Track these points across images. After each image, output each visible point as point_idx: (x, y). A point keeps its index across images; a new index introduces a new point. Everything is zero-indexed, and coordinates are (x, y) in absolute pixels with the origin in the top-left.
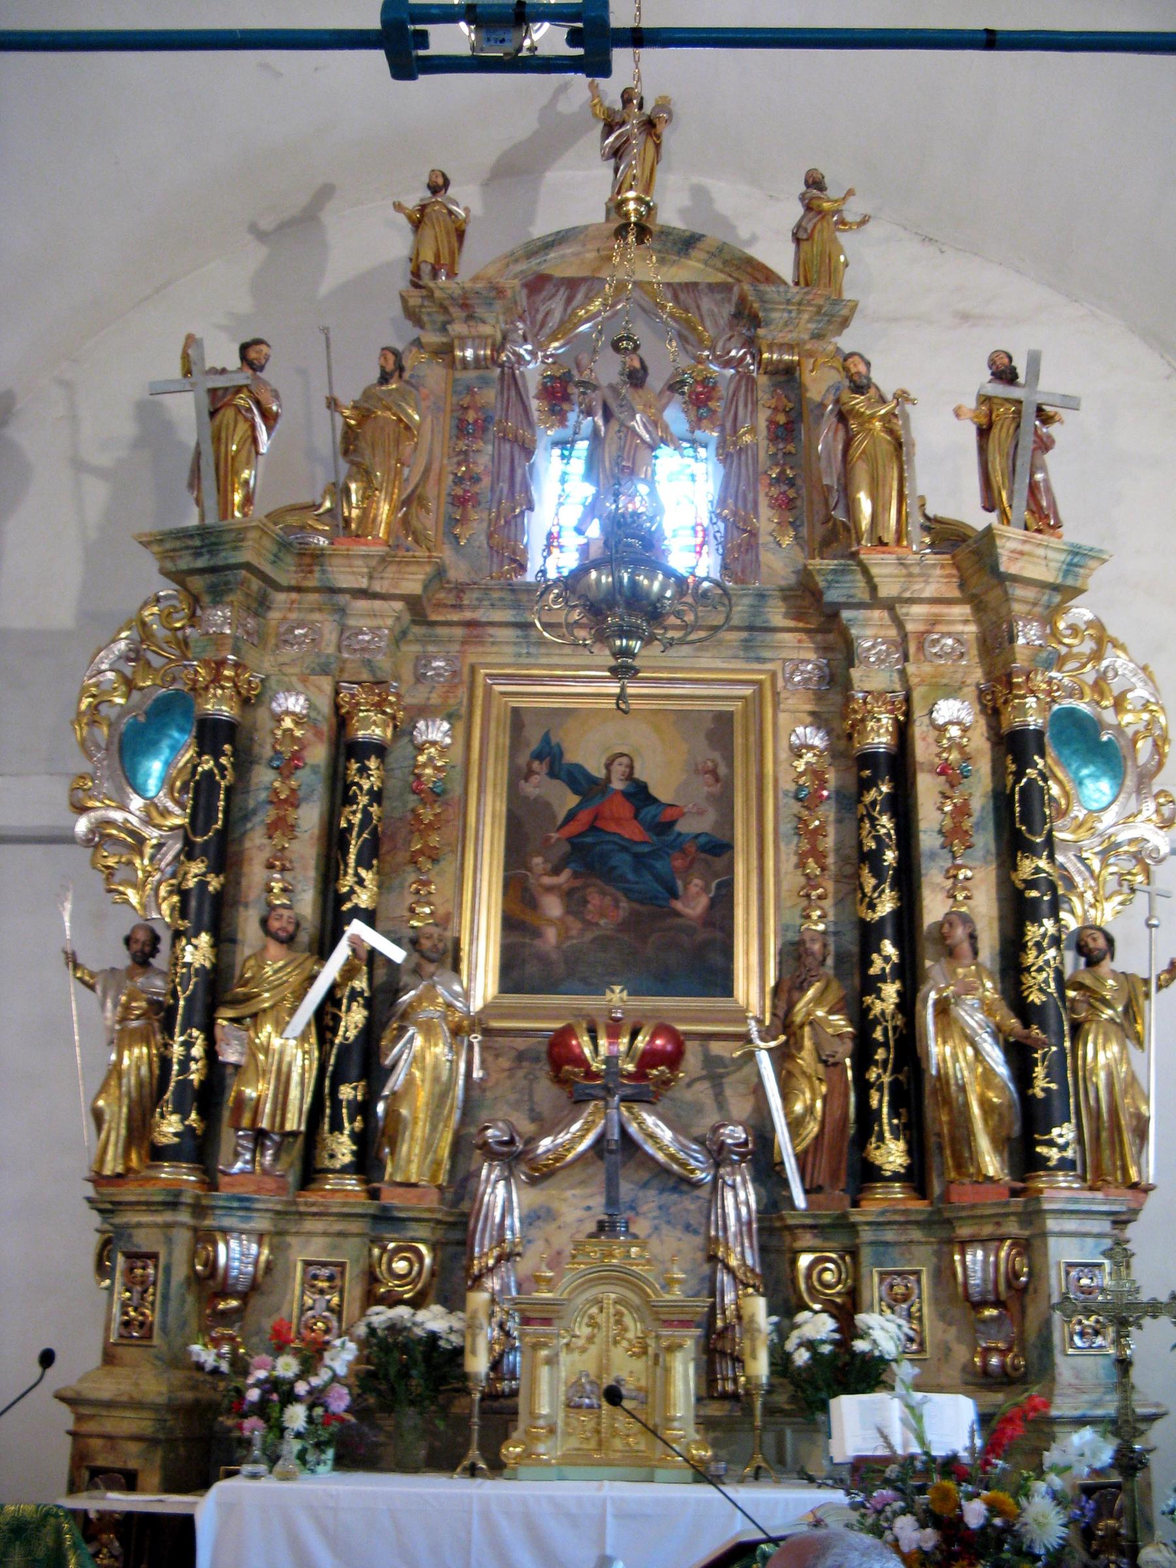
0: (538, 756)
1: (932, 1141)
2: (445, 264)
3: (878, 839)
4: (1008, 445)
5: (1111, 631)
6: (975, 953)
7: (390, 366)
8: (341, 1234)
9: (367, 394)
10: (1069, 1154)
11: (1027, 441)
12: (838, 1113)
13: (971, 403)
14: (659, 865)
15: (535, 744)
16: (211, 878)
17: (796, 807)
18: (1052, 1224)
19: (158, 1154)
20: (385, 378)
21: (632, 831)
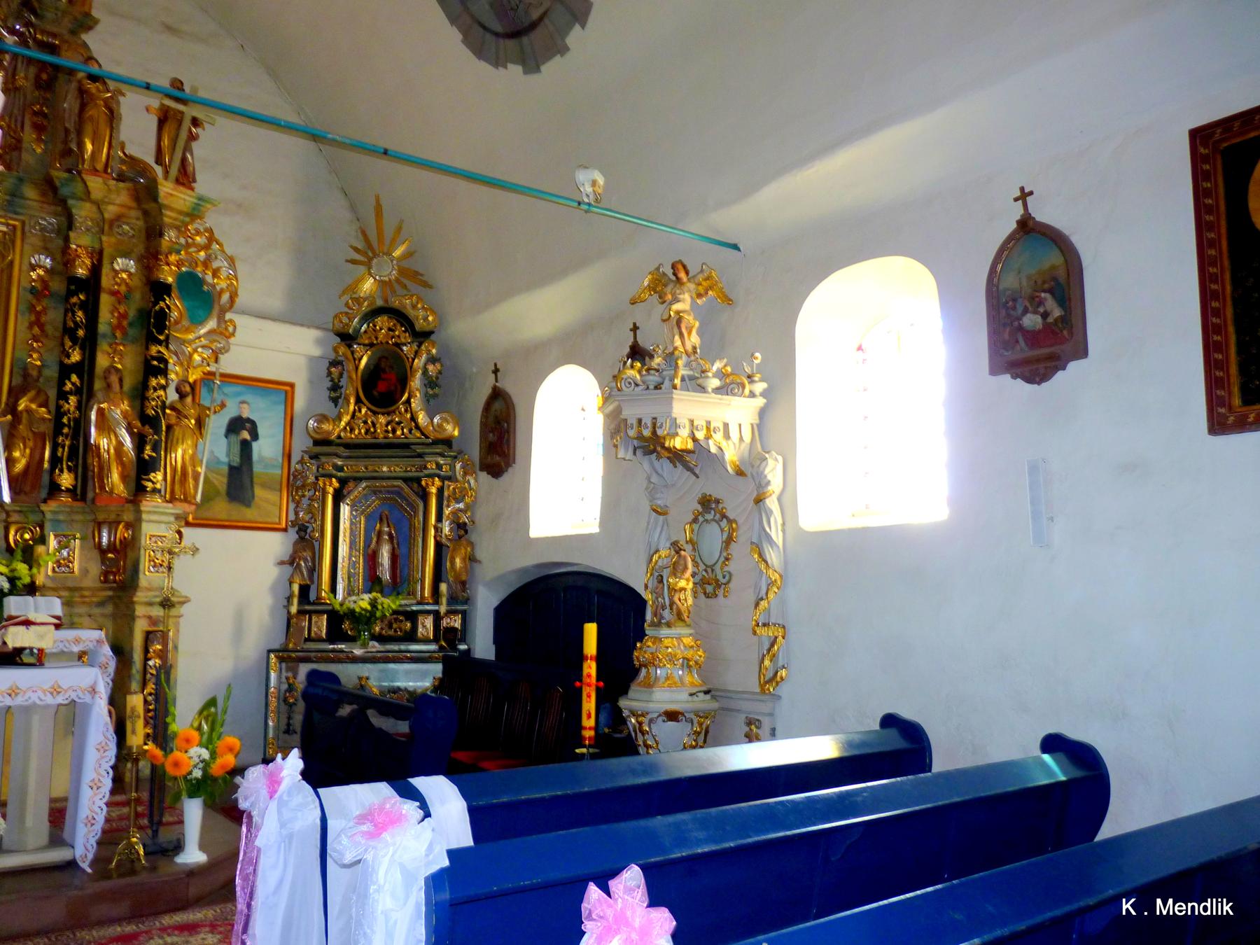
1: (90, 473)
5: (217, 235)
6: (121, 387)
10: (158, 486)
11: (183, 135)
12: (37, 457)
17: (30, 297)
18: (144, 516)
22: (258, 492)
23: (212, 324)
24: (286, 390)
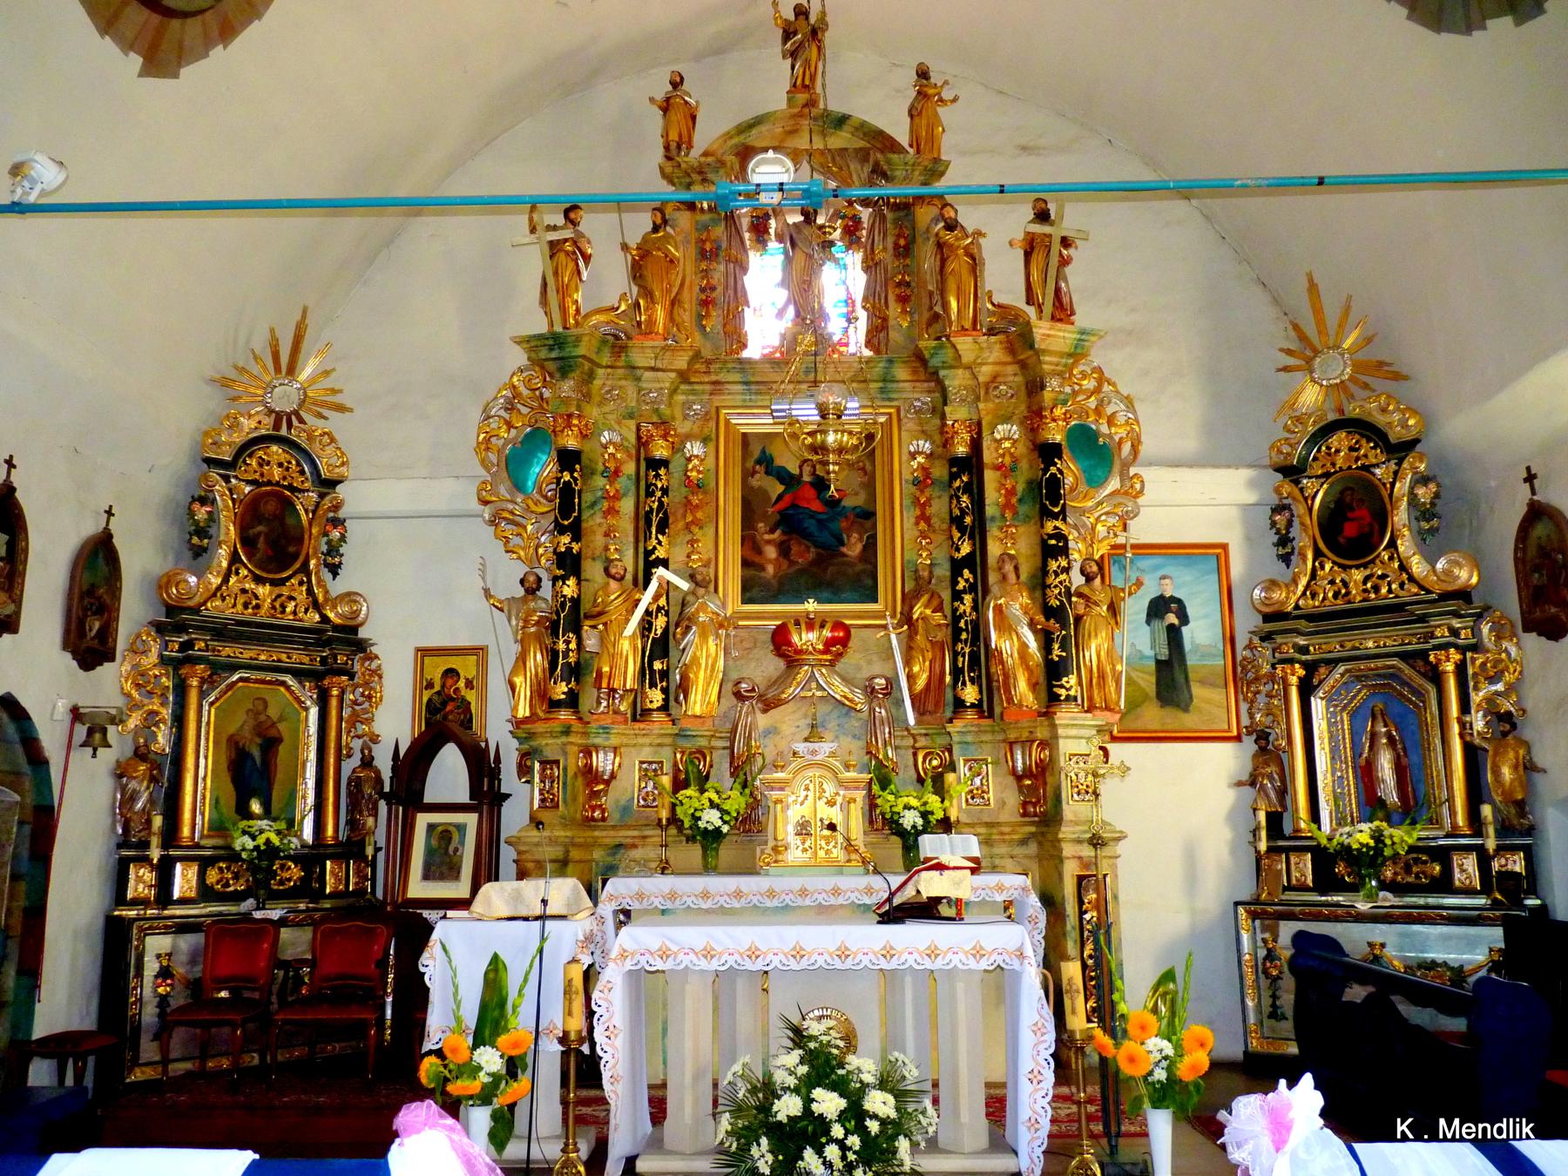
0: (759, 462)
2: (685, 143)
3: (961, 509)
4: (1041, 265)
7: (659, 221)
8: (659, 745)
9: (645, 239)
10: (1072, 693)
11: (1054, 261)
13: (1021, 236)
14: (831, 525)
15: (756, 454)
16: (574, 545)
17: (913, 489)
18: (1060, 731)
19: (555, 705)
20: (656, 229)
21: (816, 506)
22: (1196, 690)
23: (1114, 484)
24: (1219, 553)
